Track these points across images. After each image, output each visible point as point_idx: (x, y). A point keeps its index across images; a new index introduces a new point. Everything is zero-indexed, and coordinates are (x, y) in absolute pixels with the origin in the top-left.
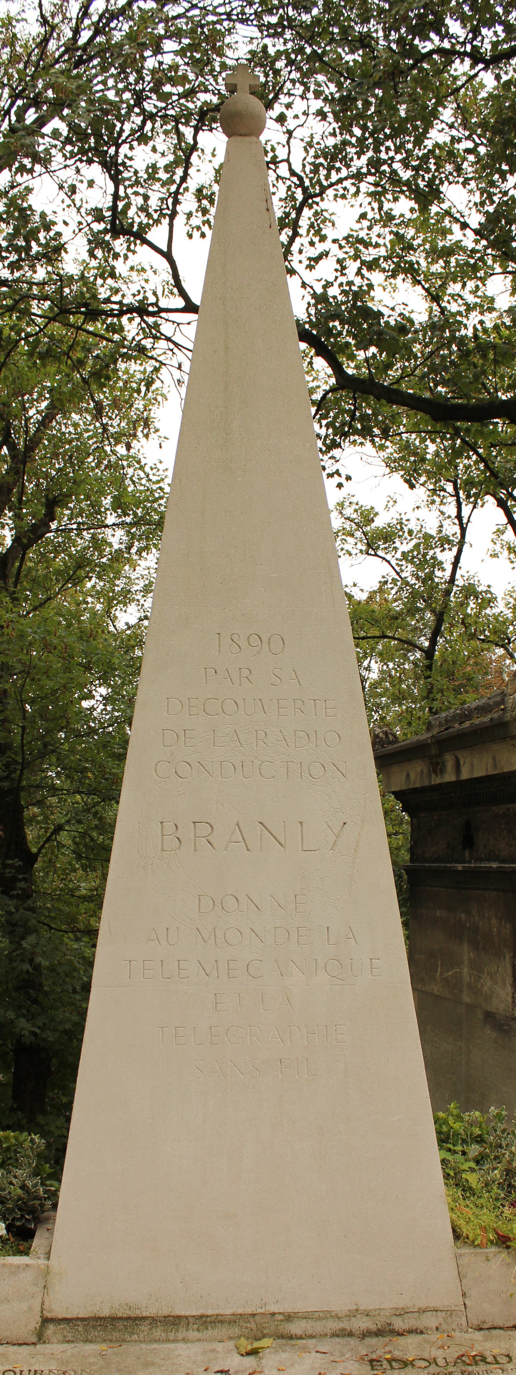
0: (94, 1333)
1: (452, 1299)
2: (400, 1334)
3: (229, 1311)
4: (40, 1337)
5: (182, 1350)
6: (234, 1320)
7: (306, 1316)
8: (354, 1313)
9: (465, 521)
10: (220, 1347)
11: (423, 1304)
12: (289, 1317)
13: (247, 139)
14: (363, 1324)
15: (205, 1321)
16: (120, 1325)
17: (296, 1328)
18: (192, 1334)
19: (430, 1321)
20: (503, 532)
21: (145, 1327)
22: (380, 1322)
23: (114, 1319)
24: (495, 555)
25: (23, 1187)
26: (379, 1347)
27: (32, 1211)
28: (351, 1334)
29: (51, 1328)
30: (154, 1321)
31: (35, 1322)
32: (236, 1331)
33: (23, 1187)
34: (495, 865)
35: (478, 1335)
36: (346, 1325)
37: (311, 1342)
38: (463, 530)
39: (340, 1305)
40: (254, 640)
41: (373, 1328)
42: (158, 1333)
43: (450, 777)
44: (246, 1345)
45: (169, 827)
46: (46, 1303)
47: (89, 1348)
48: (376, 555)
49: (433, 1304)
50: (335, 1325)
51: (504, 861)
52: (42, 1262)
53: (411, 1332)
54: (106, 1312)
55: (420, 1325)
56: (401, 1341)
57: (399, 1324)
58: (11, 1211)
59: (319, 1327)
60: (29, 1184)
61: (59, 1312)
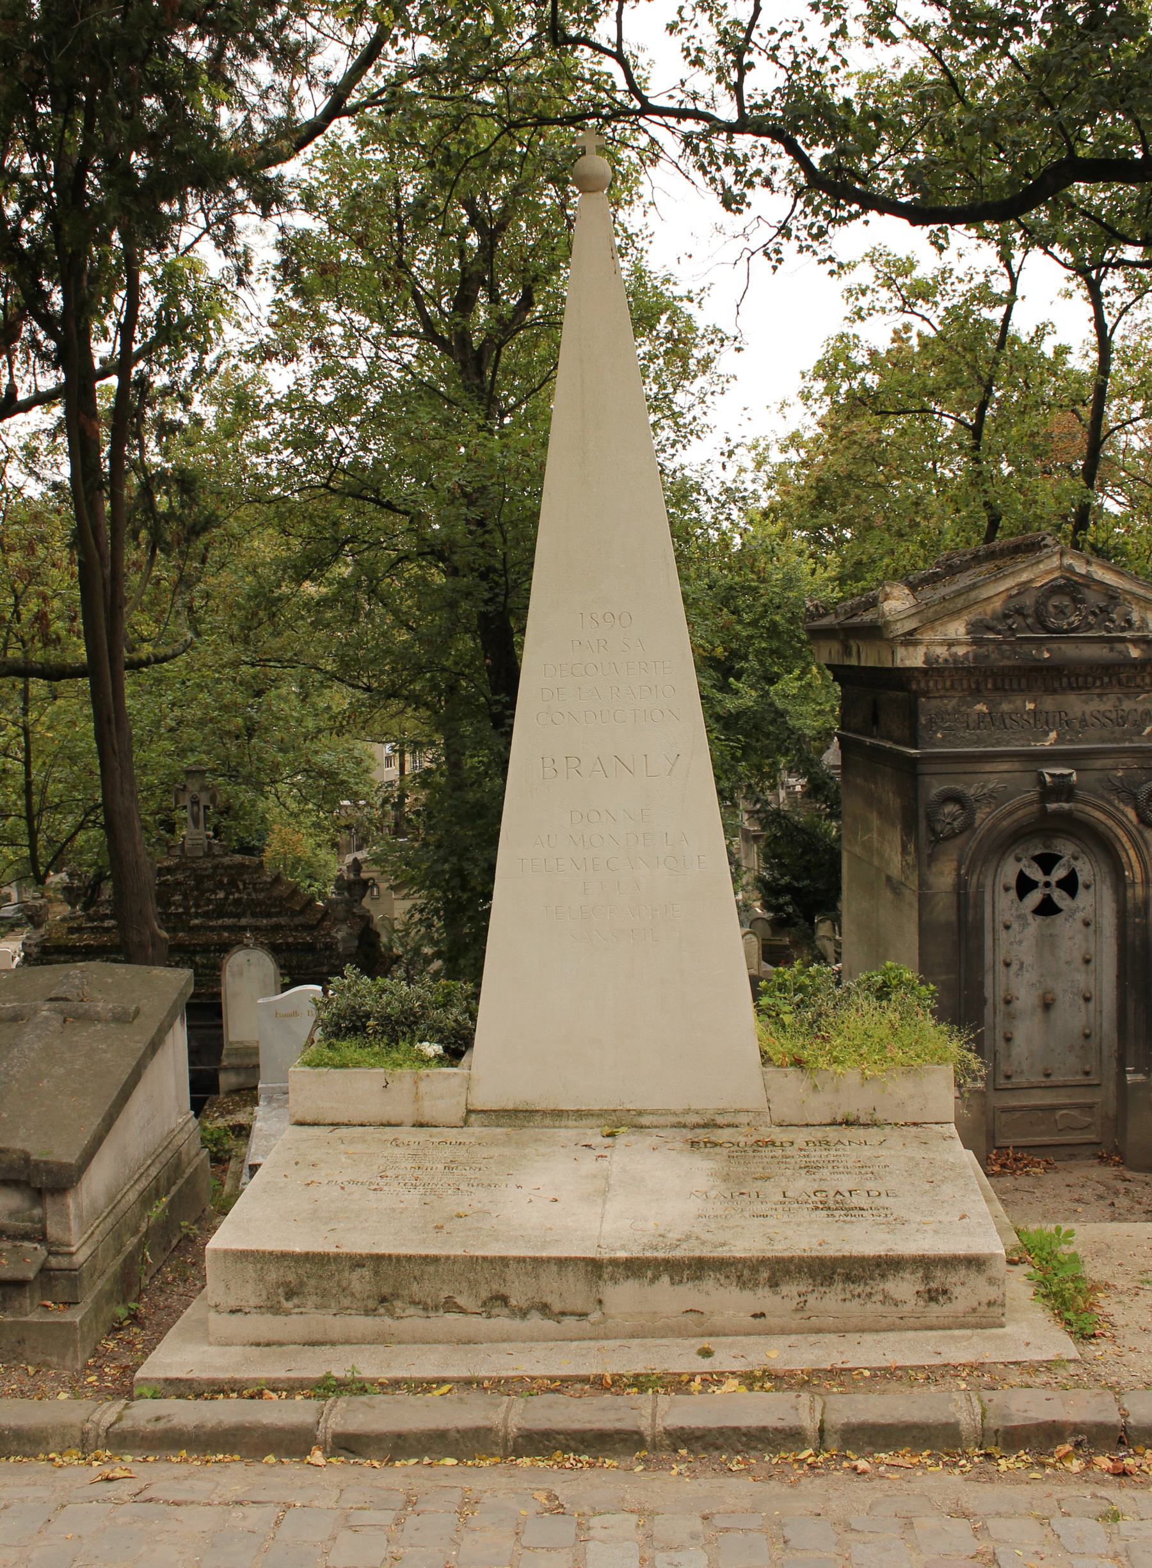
0: (503, 1121)
1: (759, 1104)
2: (720, 1127)
3: (597, 1108)
4: (466, 1123)
5: (563, 1132)
6: (601, 1114)
7: (653, 1113)
8: (687, 1111)
9: (1015, 269)
10: (589, 1132)
11: (738, 1106)
12: (640, 1113)
13: (595, 195)
14: (693, 1119)
15: (580, 1114)
16: (521, 1115)
17: (645, 1120)
18: (571, 1123)
19: (743, 1119)
20: (237, 1091)
21: (538, 1118)
22: (707, 1118)
23: (516, 1111)
24: (1069, 295)
25: (456, 1021)
26: (702, 1134)
27: (463, 1038)
28: (685, 1126)
29: (473, 1117)
30: (544, 1113)
31: (462, 1112)
32: (602, 1121)
33: (456, 1021)
34: (888, 745)
35: (778, 1129)
36: (682, 1120)
37: (655, 1131)
38: (1014, 281)
39: (676, 1105)
40: (608, 617)
41: (701, 1122)
42: (548, 1121)
43: (853, 662)
44: (607, 1130)
45: (548, 761)
46: (1070, 1079)
47: (499, 1130)
48: (913, 312)
49: (745, 1106)
50: (674, 1120)
51: (896, 742)
52: (466, 1071)
53: (728, 1126)
54: (510, 1107)
55: (736, 1121)
56: (720, 1131)
57: (720, 1120)
58: (447, 1038)
59: (662, 1120)
60: (460, 1018)
61: (479, 1106)
